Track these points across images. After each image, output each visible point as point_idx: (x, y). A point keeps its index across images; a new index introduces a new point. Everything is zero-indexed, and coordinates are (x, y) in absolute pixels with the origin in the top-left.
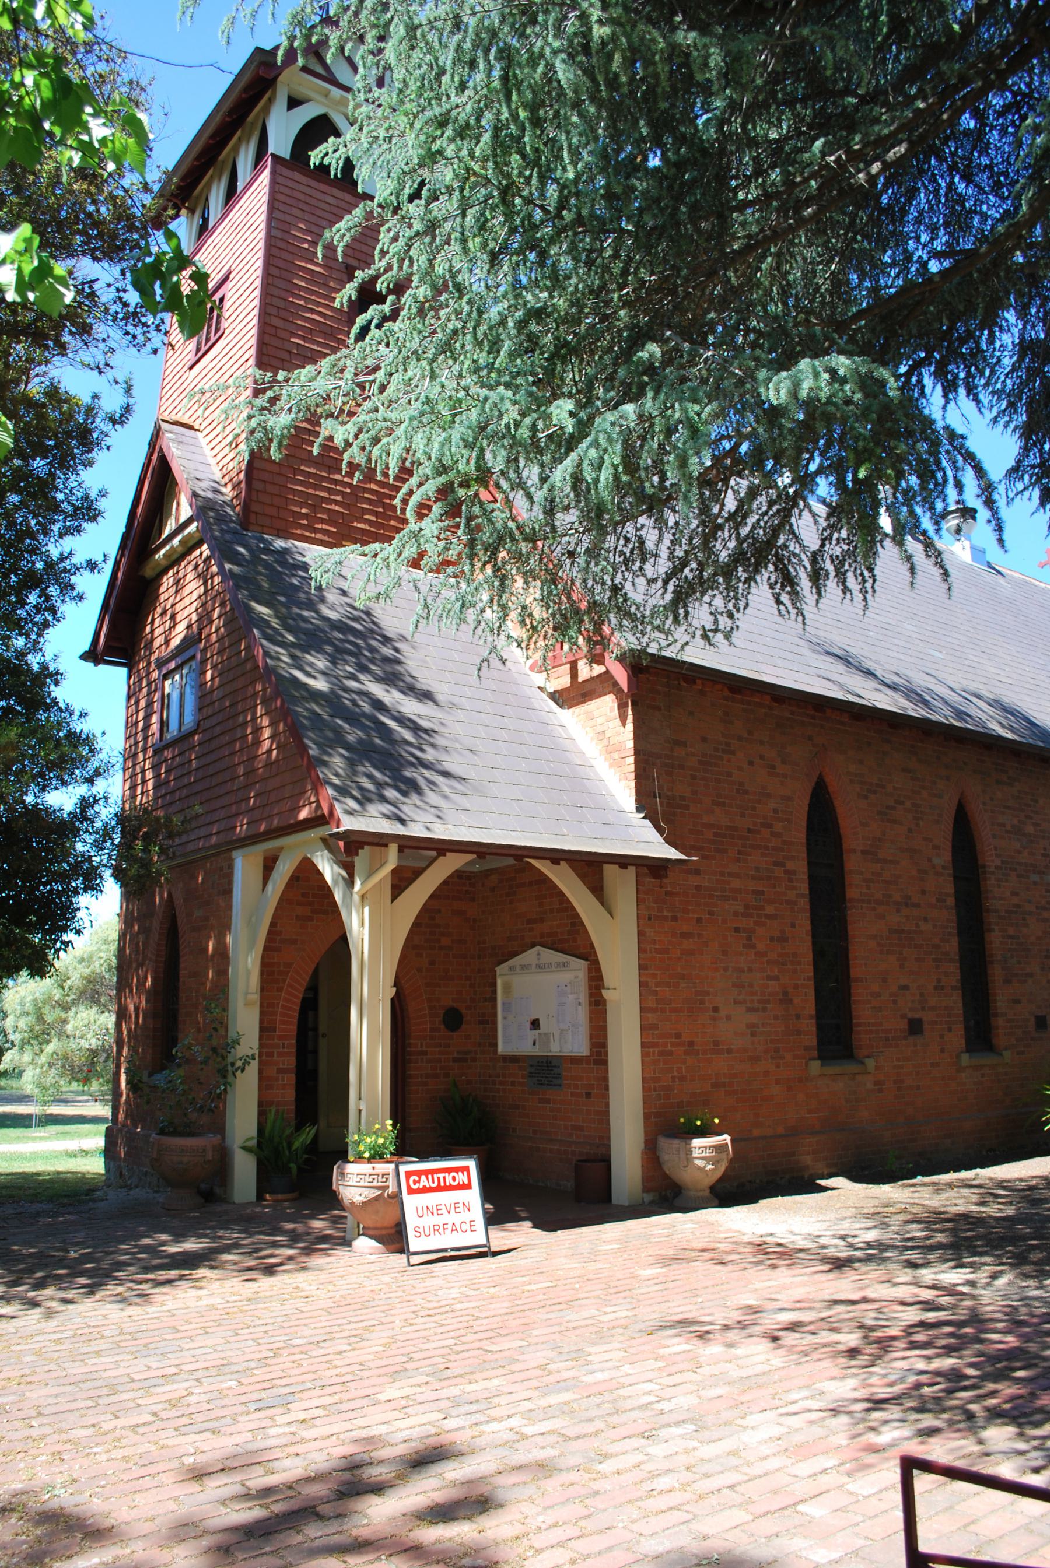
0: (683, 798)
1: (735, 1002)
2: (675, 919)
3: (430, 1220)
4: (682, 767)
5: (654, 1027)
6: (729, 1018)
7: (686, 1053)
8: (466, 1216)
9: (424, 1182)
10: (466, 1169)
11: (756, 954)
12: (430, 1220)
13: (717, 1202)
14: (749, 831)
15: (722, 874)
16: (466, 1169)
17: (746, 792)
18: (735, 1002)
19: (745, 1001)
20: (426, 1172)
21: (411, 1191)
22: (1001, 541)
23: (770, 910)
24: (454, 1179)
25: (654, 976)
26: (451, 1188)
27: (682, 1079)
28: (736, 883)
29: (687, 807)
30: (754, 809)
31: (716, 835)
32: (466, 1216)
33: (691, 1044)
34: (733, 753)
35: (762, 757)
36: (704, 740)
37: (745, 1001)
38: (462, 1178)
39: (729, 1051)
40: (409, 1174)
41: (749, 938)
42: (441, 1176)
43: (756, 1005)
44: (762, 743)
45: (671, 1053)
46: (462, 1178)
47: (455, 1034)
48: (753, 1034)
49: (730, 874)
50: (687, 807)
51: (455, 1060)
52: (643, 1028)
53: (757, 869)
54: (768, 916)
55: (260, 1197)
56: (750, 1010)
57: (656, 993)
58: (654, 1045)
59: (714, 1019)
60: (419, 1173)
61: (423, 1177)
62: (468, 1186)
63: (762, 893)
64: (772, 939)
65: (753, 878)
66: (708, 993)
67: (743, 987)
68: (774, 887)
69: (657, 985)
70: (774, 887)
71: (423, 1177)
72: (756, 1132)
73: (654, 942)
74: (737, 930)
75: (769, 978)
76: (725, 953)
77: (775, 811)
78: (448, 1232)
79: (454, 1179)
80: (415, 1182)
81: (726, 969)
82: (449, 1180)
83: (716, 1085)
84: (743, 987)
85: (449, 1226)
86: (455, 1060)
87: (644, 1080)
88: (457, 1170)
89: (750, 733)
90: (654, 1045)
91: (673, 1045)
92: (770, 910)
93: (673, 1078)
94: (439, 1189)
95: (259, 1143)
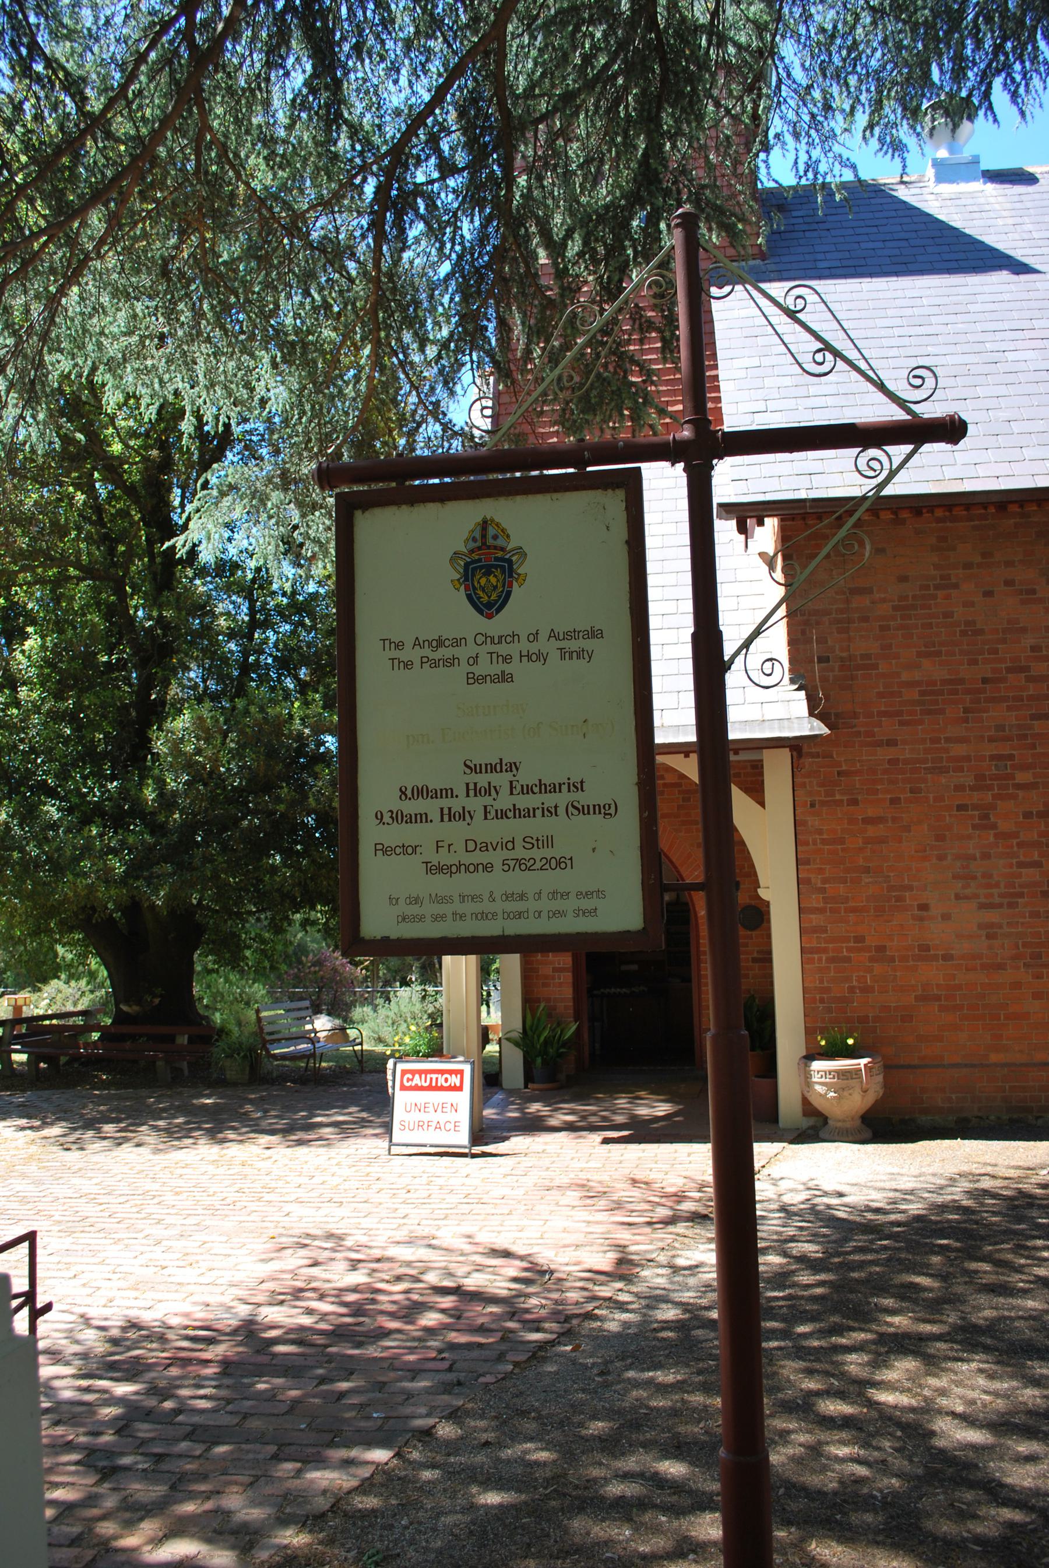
0: (867, 656)
1: (958, 897)
2: (854, 802)
3: (416, 1116)
4: (866, 619)
5: (815, 930)
6: (946, 917)
7: (872, 959)
8: (452, 1116)
9: (417, 1080)
10: (461, 1072)
11: (996, 835)
12: (416, 1116)
13: (868, 1134)
14: (985, 681)
15: (933, 741)
16: (461, 1072)
17: (981, 632)
18: (958, 897)
19: (976, 896)
20: (420, 1072)
21: (403, 1088)
22: (1020, 268)
23: (1022, 777)
24: (446, 1080)
25: (821, 871)
26: (442, 1088)
27: (866, 990)
28: (959, 750)
29: (875, 667)
30: (996, 651)
31: (922, 693)
32: (452, 1116)
33: (881, 949)
34: (956, 586)
35: (1008, 583)
36: (903, 579)
37: (976, 896)
38: (455, 1080)
39: (947, 957)
40: (404, 1072)
41: (986, 817)
42: (434, 1076)
43: (997, 900)
44: (1009, 564)
45: (848, 960)
46: (455, 1080)
47: (754, 933)
48: (989, 937)
49: (948, 740)
50: (875, 667)
51: (754, 960)
52: (802, 931)
53: (1000, 728)
54: (1018, 786)
55: (526, 1087)
56: (982, 906)
57: (823, 890)
58: (819, 950)
59: (921, 919)
60: (413, 1072)
61: (417, 1076)
62: (460, 1088)
63: (1011, 757)
64: (1027, 815)
65: (991, 740)
66: (910, 888)
67: (974, 878)
68: (1033, 746)
69: (825, 881)
70: (1033, 746)
71: (417, 1076)
72: (994, 1058)
73: (820, 832)
74: (961, 808)
75: (1021, 865)
76: (940, 838)
77: (1033, 649)
78: (431, 1129)
79: (446, 1080)
80: (408, 1080)
81: (941, 858)
82: (441, 1081)
83: (922, 998)
84: (974, 878)
85: (434, 1124)
86: (754, 960)
87: (805, 990)
88: (451, 1072)
89: (984, 555)
90: (819, 950)
91: (849, 949)
92: (1022, 777)
93: (852, 990)
94: (430, 1088)
95: (523, 1039)
